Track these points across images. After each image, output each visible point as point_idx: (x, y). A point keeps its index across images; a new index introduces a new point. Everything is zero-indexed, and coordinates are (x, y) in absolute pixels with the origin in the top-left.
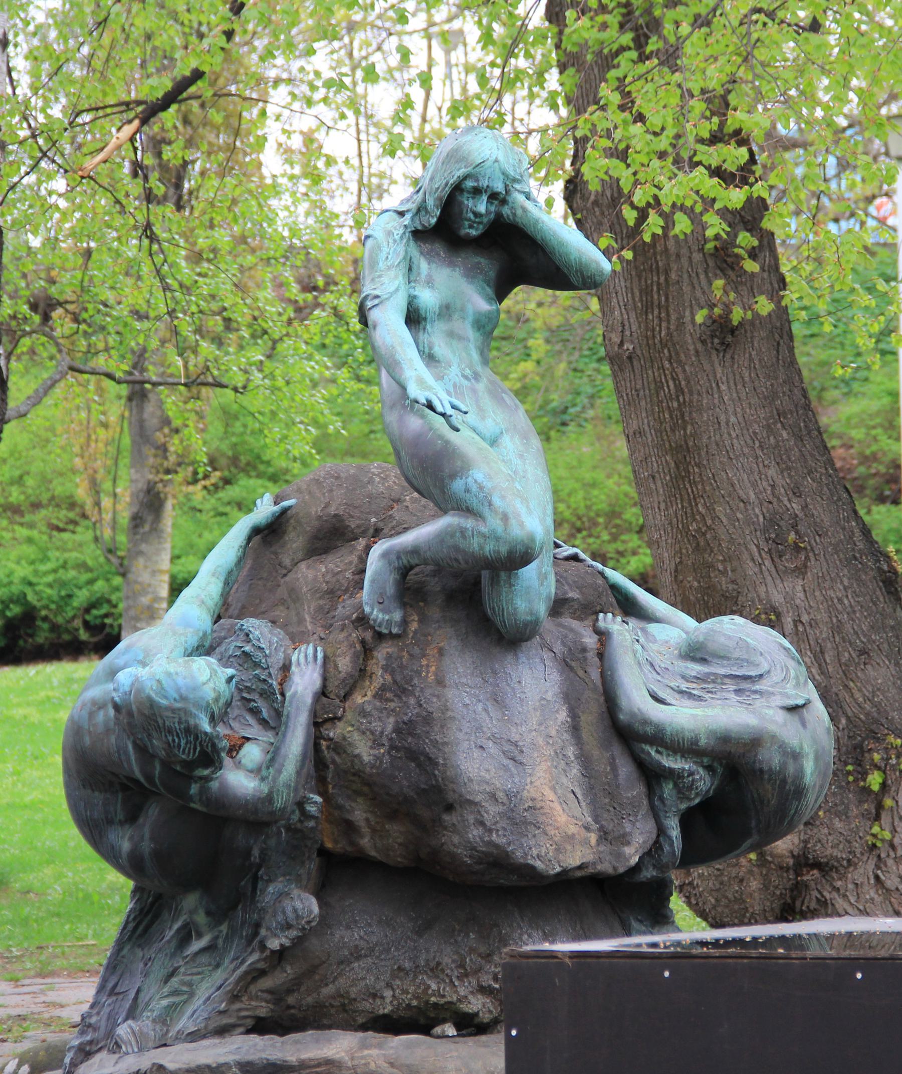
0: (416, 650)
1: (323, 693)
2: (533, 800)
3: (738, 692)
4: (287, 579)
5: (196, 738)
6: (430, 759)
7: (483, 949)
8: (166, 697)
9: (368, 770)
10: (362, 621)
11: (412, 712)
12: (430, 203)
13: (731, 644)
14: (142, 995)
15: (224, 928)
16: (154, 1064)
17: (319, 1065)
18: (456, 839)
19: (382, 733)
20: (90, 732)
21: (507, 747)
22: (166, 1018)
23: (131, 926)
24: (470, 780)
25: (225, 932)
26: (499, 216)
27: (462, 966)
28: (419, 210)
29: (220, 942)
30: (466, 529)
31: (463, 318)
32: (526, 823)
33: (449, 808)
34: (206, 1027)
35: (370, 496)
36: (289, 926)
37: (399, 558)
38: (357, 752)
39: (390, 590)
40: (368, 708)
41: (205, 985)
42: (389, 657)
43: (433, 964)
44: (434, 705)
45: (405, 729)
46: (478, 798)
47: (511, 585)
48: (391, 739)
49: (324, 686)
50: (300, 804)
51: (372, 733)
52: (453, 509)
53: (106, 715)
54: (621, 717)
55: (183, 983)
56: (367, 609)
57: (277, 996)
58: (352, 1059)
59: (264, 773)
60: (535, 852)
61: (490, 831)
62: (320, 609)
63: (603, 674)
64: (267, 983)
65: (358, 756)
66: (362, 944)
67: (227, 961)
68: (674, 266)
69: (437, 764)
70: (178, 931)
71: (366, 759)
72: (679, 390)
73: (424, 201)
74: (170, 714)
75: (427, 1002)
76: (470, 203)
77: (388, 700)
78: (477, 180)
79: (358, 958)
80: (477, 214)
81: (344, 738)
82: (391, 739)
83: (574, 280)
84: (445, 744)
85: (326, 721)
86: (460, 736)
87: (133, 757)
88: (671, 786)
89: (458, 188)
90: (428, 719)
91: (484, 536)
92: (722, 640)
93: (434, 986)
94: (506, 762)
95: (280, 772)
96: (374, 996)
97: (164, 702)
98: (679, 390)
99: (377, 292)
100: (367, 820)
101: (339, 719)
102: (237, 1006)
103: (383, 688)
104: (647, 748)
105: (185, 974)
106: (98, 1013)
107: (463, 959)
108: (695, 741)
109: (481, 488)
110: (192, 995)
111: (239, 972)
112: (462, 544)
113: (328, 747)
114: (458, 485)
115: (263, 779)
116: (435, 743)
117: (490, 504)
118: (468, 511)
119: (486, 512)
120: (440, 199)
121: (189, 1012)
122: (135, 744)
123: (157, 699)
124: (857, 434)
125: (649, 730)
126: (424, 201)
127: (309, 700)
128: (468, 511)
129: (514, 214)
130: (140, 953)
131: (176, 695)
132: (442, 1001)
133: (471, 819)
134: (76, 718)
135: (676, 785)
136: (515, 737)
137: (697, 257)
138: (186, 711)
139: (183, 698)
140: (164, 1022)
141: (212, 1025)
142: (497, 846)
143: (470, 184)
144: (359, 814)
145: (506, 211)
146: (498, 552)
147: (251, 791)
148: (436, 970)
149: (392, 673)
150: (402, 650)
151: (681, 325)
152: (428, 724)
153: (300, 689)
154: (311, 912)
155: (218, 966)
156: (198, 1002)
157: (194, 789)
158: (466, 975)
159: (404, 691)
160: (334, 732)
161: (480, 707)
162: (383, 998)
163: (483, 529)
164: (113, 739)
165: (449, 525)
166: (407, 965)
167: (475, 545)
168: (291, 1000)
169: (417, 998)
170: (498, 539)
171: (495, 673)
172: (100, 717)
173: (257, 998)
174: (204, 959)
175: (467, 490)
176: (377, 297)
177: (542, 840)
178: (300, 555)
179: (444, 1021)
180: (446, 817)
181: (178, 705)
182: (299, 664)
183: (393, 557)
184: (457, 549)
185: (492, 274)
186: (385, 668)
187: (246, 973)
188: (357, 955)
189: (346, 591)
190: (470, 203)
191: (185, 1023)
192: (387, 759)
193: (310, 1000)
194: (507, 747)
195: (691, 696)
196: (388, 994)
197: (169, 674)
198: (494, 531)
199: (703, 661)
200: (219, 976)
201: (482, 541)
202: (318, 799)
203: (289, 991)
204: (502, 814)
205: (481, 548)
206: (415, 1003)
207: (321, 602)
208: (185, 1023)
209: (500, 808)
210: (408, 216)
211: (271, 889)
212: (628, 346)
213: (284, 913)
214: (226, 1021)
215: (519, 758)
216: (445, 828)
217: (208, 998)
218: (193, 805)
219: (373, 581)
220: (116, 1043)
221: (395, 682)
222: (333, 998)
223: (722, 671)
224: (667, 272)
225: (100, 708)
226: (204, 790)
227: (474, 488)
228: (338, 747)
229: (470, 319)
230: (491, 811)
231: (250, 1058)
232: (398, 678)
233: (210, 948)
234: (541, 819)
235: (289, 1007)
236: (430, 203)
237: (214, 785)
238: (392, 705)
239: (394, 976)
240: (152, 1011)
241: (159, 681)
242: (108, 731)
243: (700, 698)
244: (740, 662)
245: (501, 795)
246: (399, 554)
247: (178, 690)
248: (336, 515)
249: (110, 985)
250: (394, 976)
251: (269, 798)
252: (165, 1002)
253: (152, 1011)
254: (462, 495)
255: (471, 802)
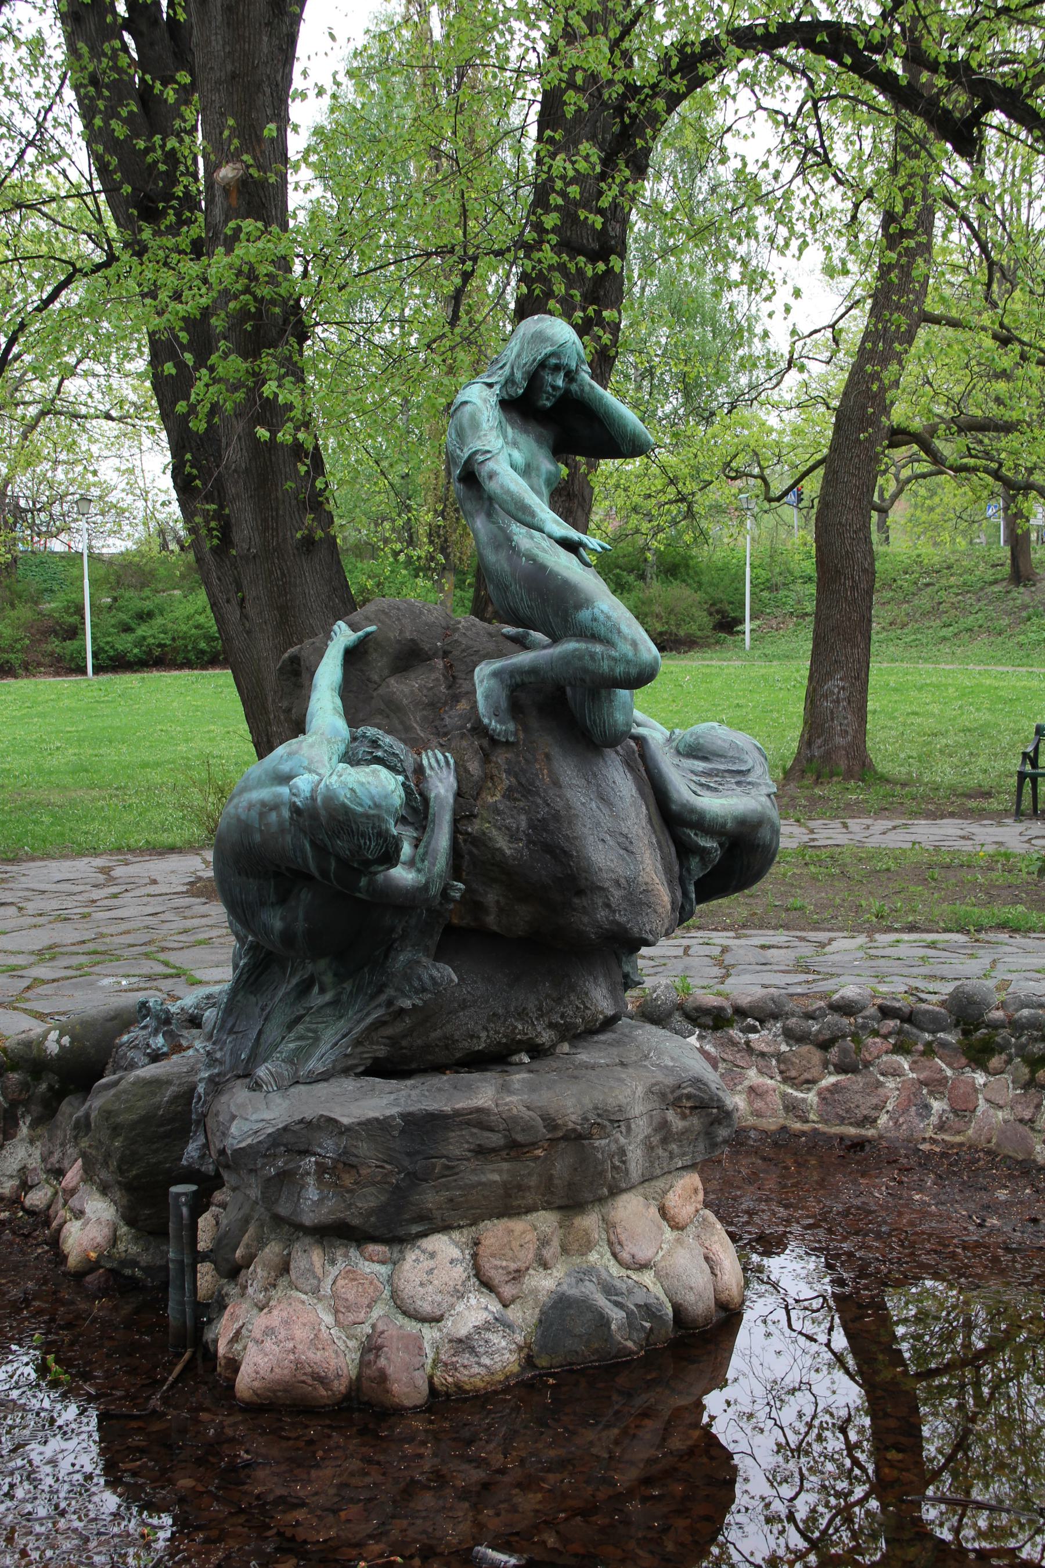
0: (529, 756)
1: (459, 794)
2: (646, 884)
3: (738, 783)
4: (380, 691)
5: (385, 840)
6: (565, 852)
7: (555, 995)
8: (361, 805)
9: (511, 861)
10: (479, 730)
11: (543, 811)
12: (518, 375)
13: (727, 745)
14: (264, 1037)
15: (348, 986)
16: (322, 1116)
17: (471, 1113)
18: (586, 919)
19: (518, 829)
20: (261, 831)
21: (621, 839)
22: (295, 1059)
23: (244, 977)
24: (601, 870)
25: (348, 990)
26: (567, 391)
27: (540, 1009)
28: (506, 382)
29: (344, 997)
30: (596, 653)
31: (538, 476)
32: (641, 903)
33: (580, 893)
34: (333, 1068)
35: (427, 624)
36: (424, 990)
37: (512, 676)
38: (498, 846)
39: (504, 704)
40: (501, 807)
41: (330, 1032)
42: (508, 761)
43: (520, 1010)
44: (559, 804)
45: (538, 826)
46: (607, 885)
47: (611, 701)
48: (528, 835)
49: (459, 788)
50: (444, 893)
51: (508, 829)
52: (574, 635)
53: (279, 815)
54: (674, 807)
55: (309, 1030)
56: (486, 721)
57: (393, 1041)
58: (497, 1105)
59: (419, 865)
60: (648, 928)
61: (614, 912)
62: (425, 718)
63: (647, 771)
64: (389, 1031)
65: (500, 850)
66: (469, 997)
67: (350, 1013)
68: (281, 507)
69: (572, 856)
70: (297, 985)
71: (508, 852)
72: (283, 575)
73: (512, 374)
74: (364, 820)
75: (513, 1039)
76: (550, 379)
77: (515, 800)
78: (559, 358)
79: (463, 1009)
80: (555, 388)
81: (484, 834)
82: (528, 835)
83: (624, 449)
84: (576, 838)
85: (463, 817)
86: (586, 831)
87: (310, 854)
88: (697, 860)
89: (543, 365)
90: (556, 817)
91: (614, 659)
92: (719, 742)
93: (520, 1027)
94: (622, 852)
95: (434, 865)
96: (472, 1037)
97: (360, 809)
98: (283, 575)
99: (487, 448)
100: (498, 902)
101: (475, 816)
102: (360, 1049)
103: (510, 789)
104: (688, 831)
105: (310, 1022)
106: (221, 1049)
107: (541, 1004)
108: (724, 825)
109: (608, 618)
110: (317, 1039)
111: (363, 1025)
112: (591, 666)
113: (465, 841)
114: (584, 615)
115: (419, 871)
116: (567, 838)
117: (619, 632)
118: (594, 637)
119: (615, 638)
120: (528, 372)
121: (317, 1054)
122: (313, 844)
123: (353, 806)
124: (56, 615)
125: (694, 817)
126: (512, 374)
127: (451, 800)
128: (594, 637)
129: (582, 391)
130: (253, 999)
131: (370, 803)
132: (525, 1038)
133: (600, 902)
134: (243, 817)
135: (702, 859)
136: (625, 831)
137: (294, 502)
138: (380, 818)
139: (377, 806)
140: (292, 1062)
141: (339, 1067)
142: (618, 924)
143: (553, 361)
144: (491, 897)
145: (574, 387)
146: (628, 673)
147: (410, 882)
148: (522, 1014)
149: (516, 776)
150: (518, 755)
151: (285, 540)
152: (558, 821)
153: (442, 791)
154: (452, 981)
155: (341, 1017)
156: (324, 1047)
157: (363, 882)
158: (542, 1016)
159: (529, 791)
160: (473, 828)
161: (594, 805)
162: (479, 1038)
163: (613, 653)
164: (288, 838)
165: (576, 650)
166: (500, 1011)
167: (606, 667)
168: (404, 1043)
169: (505, 1036)
170: (628, 662)
171: (595, 775)
172: (273, 817)
173: (378, 1043)
174: (328, 1011)
175: (595, 619)
176: (489, 452)
177: (653, 917)
178: (386, 672)
179: (517, 1052)
180: (576, 901)
181: (372, 812)
182: (431, 768)
183: (506, 676)
184: (585, 670)
185: (551, 442)
186: (508, 772)
187: (372, 1024)
188: (464, 1006)
189: (445, 704)
190: (550, 379)
191: (314, 1064)
192: (526, 852)
193: (419, 1042)
194: (621, 839)
195: (709, 788)
196: (483, 1035)
197: (362, 784)
198: (625, 655)
199: (705, 759)
200: (342, 1025)
201: (612, 663)
202: (461, 886)
203: (404, 1036)
204: (624, 898)
205: (612, 670)
206: (504, 1040)
207: (425, 713)
208: (314, 1064)
209: (622, 892)
210: (497, 387)
211: (401, 958)
212: (253, 550)
213: (420, 979)
214: (351, 1062)
215: (630, 848)
216: (575, 910)
217: (336, 1044)
218: (358, 895)
219: (487, 697)
220: (256, 1082)
221: (520, 784)
222: (439, 1039)
223: (722, 767)
224: (277, 510)
225: (271, 810)
226: (371, 882)
227: (602, 618)
228: (479, 841)
229: (544, 477)
230: (616, 895)
231: (411, 1109)
232: (523, 781)
233: (335, 1003)
234: (652, 899)
235: (402, 1048)
236: (518, 375)
237: (380, 877)
238: (522, 804)
239: (489, 1021)
240: (281, 1052)
241: (352, 790)
242: (282, 831)
243: (716, 790)
244: (733, 760)
245: (623, 881)
246: (514, 672)
247: (372, 798)
248: (412, 640)
249: (229, 1025)
250: (489, 1021)
251: (426, 888)
252: (292, 1046)
253: (281, 1052)
254: (589, 623)
255: (602, 889)
